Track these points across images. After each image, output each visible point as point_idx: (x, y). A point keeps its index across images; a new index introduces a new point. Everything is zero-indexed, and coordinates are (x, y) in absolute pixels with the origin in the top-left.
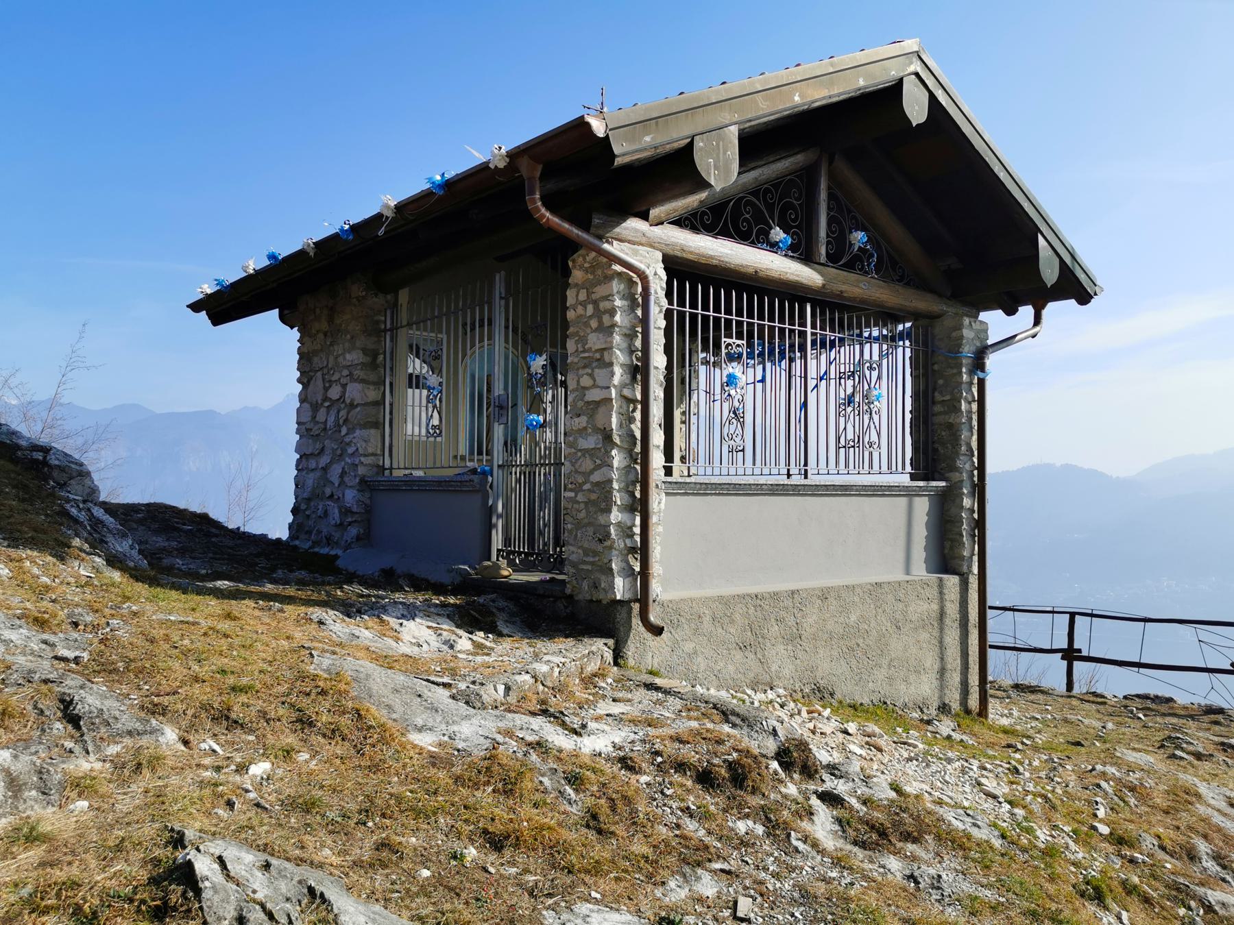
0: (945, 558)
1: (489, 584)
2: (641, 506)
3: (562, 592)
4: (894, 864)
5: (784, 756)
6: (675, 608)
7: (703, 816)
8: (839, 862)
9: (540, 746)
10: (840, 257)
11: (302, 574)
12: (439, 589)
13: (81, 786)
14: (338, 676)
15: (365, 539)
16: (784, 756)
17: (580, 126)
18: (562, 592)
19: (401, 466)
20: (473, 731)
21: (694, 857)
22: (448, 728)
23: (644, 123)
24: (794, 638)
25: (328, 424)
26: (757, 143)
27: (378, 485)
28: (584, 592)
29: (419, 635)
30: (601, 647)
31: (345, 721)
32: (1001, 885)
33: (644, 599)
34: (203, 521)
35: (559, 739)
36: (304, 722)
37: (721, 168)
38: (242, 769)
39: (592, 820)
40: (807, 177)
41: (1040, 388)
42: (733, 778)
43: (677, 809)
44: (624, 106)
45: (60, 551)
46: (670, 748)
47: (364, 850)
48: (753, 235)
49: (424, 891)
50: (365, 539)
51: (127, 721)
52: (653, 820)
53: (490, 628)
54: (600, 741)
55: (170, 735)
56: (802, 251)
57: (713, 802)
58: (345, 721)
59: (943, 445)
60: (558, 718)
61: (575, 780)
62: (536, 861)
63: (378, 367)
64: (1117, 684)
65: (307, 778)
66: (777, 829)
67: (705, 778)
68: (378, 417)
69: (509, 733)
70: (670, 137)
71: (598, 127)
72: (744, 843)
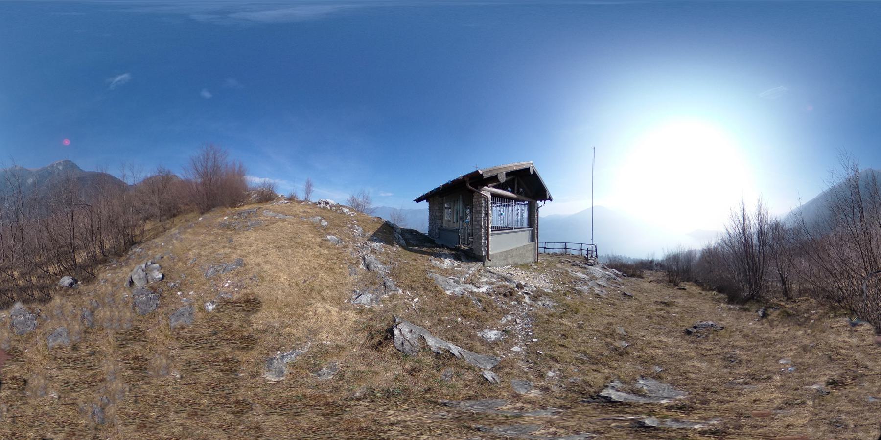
0: (533, 240)
1: (458, 249)
2: (488, 239)
3: (472, 254)
4: (540, 303)
5: (517, 287)
6: (493, 255)
7: (505, 303)
8: (532, 306)
9: (472, 293)
10: (518, 193)
11: (429, 245)
12: (451, 249)
13: (383, 301)
14: (432, 278)
15: (439, 238)
16: (517, 287)
17: (477, 172)
18: (472, 254)
19: (445, 226)
20: (458, 290)
21: (505, 313)
22: (453, 289)
23: (489, 171)
24: (512, 257)
25: (435, 217)
26: (508, 174)
27: (441, 229)
28: (477, 253)
29: (447, 263)
30: (481, 264)
31: (433, 289)
32: (557, 301)
33: (488, 255)
34: (416, 232)
35: (476, 290)
36: (425, 289)
37: (502, 179)
38: (413, 299)
39: (484, 309)
40: (513, 180)
41: (545, 209)
42: (510, 294)
43: (500, 303)
44: (484, 167)
45: (392, 245)
46: (497, 290)
47: (436, 321)
48: (506, 189)
49: (449, 330)
50: (439, 238)
51: (393, 288)
52: (497, 306)
53: (460, 260)
54: (484, 289)
55: (401, 291)
56: (513, 192)
57: (506, 300)
58: (433, 289)
59: (532, 221)
60: (474, 284)
61: (480, 301)
62: (474, 320)
63: (441, 209)
64: (552, 251)
65: (425, 303)
66: (519, 302)
67: (505, 295)
68: (440, 218)
69: (465, 290)
70: (494, 174)
71: (480, 172)
72: (514, 306)
